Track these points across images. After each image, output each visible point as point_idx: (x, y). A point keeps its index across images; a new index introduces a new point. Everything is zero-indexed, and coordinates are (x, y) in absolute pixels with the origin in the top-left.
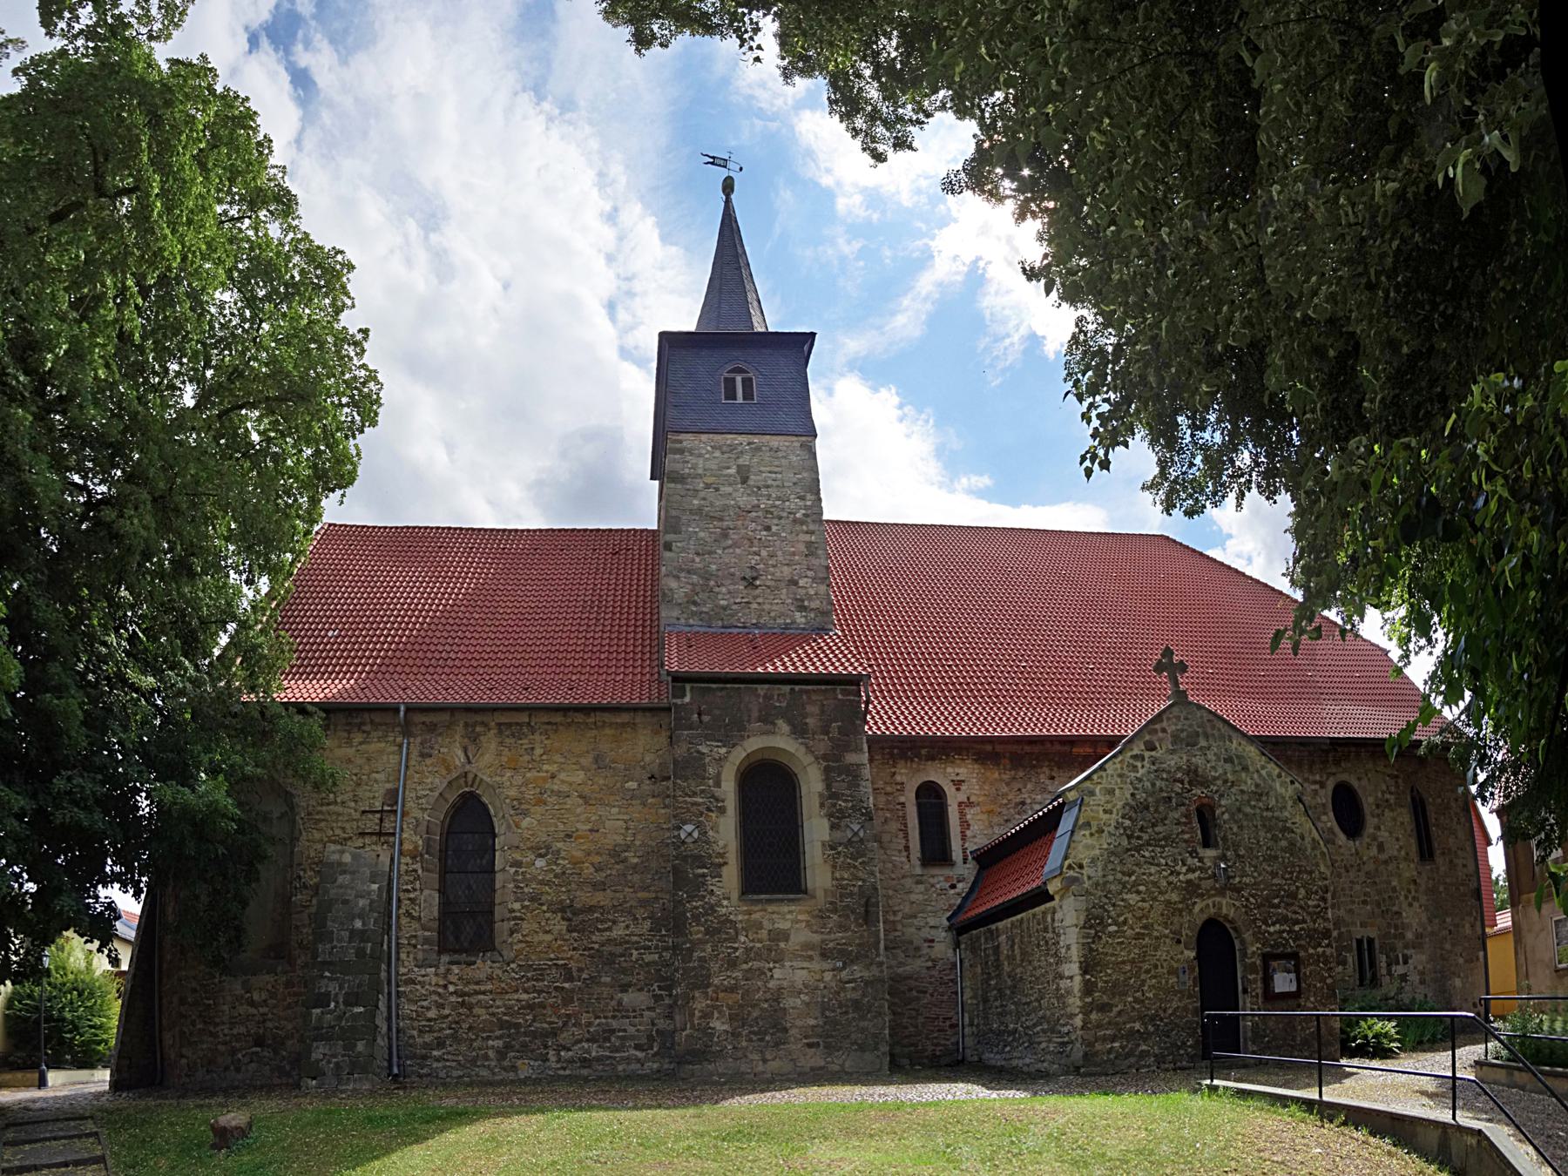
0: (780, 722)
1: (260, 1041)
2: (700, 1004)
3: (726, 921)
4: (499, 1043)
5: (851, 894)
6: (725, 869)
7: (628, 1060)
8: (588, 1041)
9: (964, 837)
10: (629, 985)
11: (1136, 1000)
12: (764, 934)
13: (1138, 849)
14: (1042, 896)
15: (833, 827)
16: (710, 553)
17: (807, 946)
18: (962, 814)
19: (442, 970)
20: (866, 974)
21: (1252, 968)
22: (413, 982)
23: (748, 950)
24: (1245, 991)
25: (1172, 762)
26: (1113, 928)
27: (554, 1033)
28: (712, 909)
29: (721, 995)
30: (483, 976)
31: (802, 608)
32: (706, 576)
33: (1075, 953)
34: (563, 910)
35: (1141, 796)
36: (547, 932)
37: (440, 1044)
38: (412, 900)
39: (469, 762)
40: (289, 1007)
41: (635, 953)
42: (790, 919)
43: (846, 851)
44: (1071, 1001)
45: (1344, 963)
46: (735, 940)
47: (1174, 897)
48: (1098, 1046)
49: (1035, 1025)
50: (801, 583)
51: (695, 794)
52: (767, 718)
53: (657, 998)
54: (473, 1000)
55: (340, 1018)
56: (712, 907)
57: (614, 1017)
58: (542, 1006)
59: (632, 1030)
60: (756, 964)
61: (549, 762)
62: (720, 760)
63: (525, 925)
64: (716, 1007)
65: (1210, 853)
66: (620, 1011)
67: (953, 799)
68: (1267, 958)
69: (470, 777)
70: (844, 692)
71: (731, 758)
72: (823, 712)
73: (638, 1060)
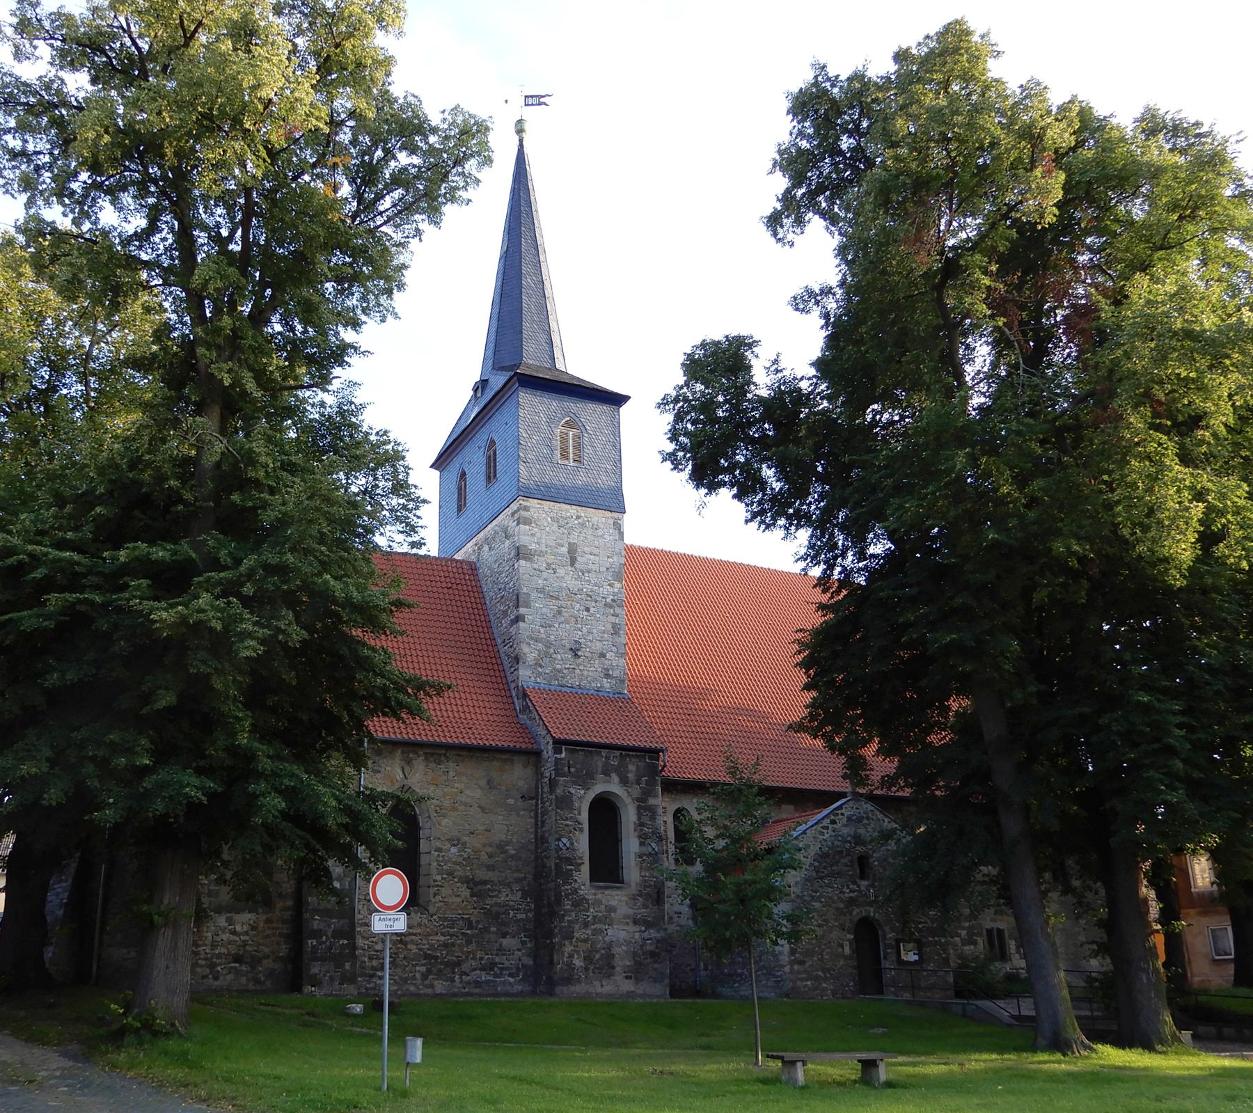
0: (614, 775)
1: (238, 959)
2: (568, 948)
3: (584, 900)
5: (650, 886)
13: (822, 878)
15: (642, 844)
16: (550, 626)
17: (626, 917)
20: (657, 935)
21: (890, 946)
23: (594, 917)
25: (845, 831)
27: (459, 964)
28: (575, 891)
31: (607, 676)
32: (548, 644)
34: (468, 882)
42: (617, 899)
43: (650, 859)
45: (975, 943)
47: (841, 905)
50: (608, 656)
53: (523, 943)
54: (408, 939)
58: (453, 945)
59: (507, 964)
62: (581, 798)
63: (443, 890)
65: (864, 883)
66: (501, 949)
68: (898, 941)
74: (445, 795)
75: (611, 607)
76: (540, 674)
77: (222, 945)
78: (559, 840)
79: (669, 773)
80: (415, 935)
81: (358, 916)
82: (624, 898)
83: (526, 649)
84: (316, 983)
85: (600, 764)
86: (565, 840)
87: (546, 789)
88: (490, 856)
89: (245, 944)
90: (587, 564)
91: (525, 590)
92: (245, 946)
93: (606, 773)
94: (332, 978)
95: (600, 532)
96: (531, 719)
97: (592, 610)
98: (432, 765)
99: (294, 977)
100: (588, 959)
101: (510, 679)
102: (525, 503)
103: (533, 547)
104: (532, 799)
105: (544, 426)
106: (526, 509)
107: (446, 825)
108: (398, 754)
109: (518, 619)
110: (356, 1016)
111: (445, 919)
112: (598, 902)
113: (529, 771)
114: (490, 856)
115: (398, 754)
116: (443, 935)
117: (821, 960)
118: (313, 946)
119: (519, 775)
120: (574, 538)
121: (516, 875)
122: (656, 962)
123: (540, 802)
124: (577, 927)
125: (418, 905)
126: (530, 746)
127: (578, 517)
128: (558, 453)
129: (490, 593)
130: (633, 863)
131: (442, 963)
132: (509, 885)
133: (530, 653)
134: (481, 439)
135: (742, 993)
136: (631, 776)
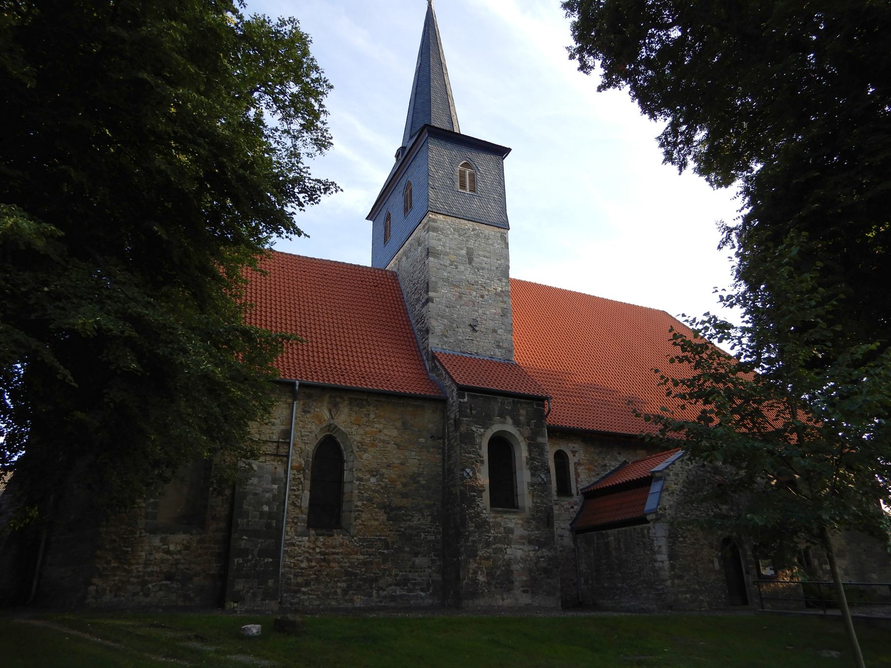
0: (508, 418)
1: (170, 577)
2: (473, 565)
3: (485, 522)
4: (344, 585)
8: (395, 585)
9: (577, 482)
14: (643, 520)
15: (533, 475)
16: (453, 307)
17: (522, 537)
18: (576, 469)
19: (313, 538)
20: (549, 553)
22: (293, 545)
23: (495, 538)
24: (748, 573)
26: (681, 539)
27: (376, 580)
28: (478, 514)
30: (337, 543)
31: (499, 347)
32: (452, 321)
33: (664, 549)
35: (691, 478)
36: (377, 520)
37: (307, 584)
38: (297, 496)
39: (333, 418)
41: (423, 535)
42: (513, 522)
43: (540, 488)
46: (489, 532)
48: (680, 596)
50: (499, 331)
51: (470, 453)
52: (502, 415)
53: (433, 561)
54: (331, 557)
57: (410, 572)
58: (371, 563)
59: (419, 580)
60: (499, 546)
61: (380, 423)
62: (481, 435)
64: (479, 568)
67: (572, 460)
69: (332, 427)
70: (538, 405)
71: (486, 434)
73: (422, 597)
74: (366, 433)
75: (500, 296)
76: (445, 343)
78: (463, 470)
79: (550, 420)
80: (337, 554)
81: (284, 537)
82: (520, 522)
83: (434, 323)
84: (238, 598)
85: (496, 408)
86: (468, 470)
87: (452, 429)
88: (404, 485)
89: (177, 562)
90: (481, 263)
93: (502, 415)
94: (254, 595)
95: (490, 242)
96: (438, 375)
97: (486, 297)
99: (219, 596)
100: (490, 574)
101: (422, 348)
102: (434, 217)
103: (440, 248)
104: (439, 438)
106: (434, 221)
108: (327, 398)
109: (429, 300)
110: (252, 638)
112: (498, 525)
114: (404, 485)
115: (327, 398)
116: (362, 554)
118: (239, 564)
119: (428, 419)
120: (471, 244)
121: (427, 502)
125: (341, 528)
126: (438, 394)
127: (474, 230)
128: (458, 184)
129: (406, 287)
130: (526, 491)
133: (437, 326)
134: (401, 188)
136: (522, 418)
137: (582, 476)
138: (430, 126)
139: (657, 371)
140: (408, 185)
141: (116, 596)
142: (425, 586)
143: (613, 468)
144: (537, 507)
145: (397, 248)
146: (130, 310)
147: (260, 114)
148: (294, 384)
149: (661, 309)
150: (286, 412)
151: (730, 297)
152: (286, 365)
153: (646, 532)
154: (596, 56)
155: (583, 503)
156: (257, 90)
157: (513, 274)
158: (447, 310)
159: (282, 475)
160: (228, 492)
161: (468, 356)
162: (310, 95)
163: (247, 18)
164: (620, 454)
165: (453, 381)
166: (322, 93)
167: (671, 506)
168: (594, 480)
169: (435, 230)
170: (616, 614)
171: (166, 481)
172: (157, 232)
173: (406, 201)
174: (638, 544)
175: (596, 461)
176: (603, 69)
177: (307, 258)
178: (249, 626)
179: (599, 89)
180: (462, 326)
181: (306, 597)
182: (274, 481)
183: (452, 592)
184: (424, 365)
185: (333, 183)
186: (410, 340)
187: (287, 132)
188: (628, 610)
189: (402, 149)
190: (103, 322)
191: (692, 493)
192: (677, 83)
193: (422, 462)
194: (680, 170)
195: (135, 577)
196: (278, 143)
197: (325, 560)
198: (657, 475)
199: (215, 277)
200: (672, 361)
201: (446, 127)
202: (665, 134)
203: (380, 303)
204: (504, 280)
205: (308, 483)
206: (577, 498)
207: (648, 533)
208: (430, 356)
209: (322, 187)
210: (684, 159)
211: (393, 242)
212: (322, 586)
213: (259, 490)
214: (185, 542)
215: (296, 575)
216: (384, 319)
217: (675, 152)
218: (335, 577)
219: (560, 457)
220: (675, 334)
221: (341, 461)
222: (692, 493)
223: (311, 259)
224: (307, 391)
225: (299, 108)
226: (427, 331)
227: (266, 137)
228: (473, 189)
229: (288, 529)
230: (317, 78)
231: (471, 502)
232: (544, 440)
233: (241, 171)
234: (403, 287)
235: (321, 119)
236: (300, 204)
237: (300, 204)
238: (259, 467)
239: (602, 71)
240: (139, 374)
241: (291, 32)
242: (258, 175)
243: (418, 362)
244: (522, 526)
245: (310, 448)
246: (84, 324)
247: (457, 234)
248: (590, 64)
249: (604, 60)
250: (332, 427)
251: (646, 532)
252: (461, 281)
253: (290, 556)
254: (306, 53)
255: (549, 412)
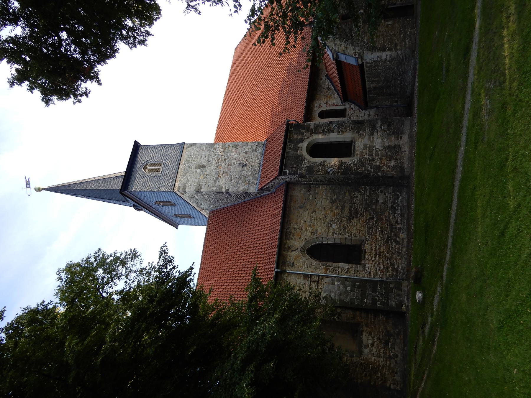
1: (387, 343)
2: (385, 168)
3: (360, 160)
4: (394, 244)
5: (354, 127)
6: (343, 161)
7: (402, 202)
8: (395, 214)
10: (376, 200)
11: (395, 36)
12: (364, 151)
13: (352, 37)
14: (361, 66)
15: (333, 132)
16: (231, 177)
17: (369, 139)
18: (330, 106)
19: (367, 262)
20: (379, 123)
23: (369, 155)
24: (395, 4)
27: (391, 225)
28: (355, 165)
29: (383, 163)
31: (256, 150)
32: (240, 178)
33: (379, 54)
36: (357, 225)
37: (393, 265)
40: (375, 326)
42: (360, 144)
43: (341, 128)
44: (393, 55)
46: (365, 159)
49: (399, 71)
50: (247, 150)
51: (319, 169)
53: (382, 192)
54: (378, 251)
55: (382, 295)
56: (355, 164)
57: (387, 205)
58: (381, 228)
59: (392, 200)
60: (374, 153)
61: (300, 222)
62: (309, 162)
63: (354, 232)
64: (386, 165)
66: (385, 203)
67: (324, 108)
69: (302, 250)
70: (291, 127)
72: (296, 134)
73: (402, 199)
75: (225, 149)
76: (253, 182)
77: (379, 351)
78: (329, 173)
79: (300, 120)
80: (376, 247)
81: (365, 278)
82: (360, 140)
83: (241, 189)
84: (400, 304)
85: (293, 152)
86: (329, 170)
88: (337, 208)
89: (379, 339)
91: (214, 189)
92: (380, 339)
93: (297, 149)
94: (399, 295)
95: (192, 154)
96: (272, 187)
97: (226, 158)
98: (291, 236)
99: (397, 315)
100: (390, 158)
101: (256, 196)
102: (177, 188)
103: (196, 185)
104: (310, 187)
105: (144, 180)
106: (179, 188)
107: (321, 229)
108: (285, 253)
110: (424, 296)
111: (368, 231)
113: (297, 188)
115: (285, 253)
116: (376, 233)
117: (395, 35)
118: (381, 304)
119: (298, 193)
120: (193, 166)
121: (347, 194)
122: (393, 124)
123: (312, 181)
124: (374, 164)
125: (361, 245)
126: (284, 188)
127: (185, 164)
128: (157, 173)
129: (219, 205)
130: (342, 136)
131: (391, 234)
132: (352, 199)
133: (243, 187)
134: (159, 208)
135: (411, 80)
136: (299, 137)
137: (334, 102)
138: (122, 190)
139: (281, 54)
140: (156, 203)
141: (397, 373)
142: (396, 197)
143: (330, 84)
144: (352, 129)
145: (195, 211)
146: (239, 367)
147: (117, 293)
148: (277, 272)
149: (234, 51)
150: (293, 277)
151: (235, 6)
152: (267, 277)
153: (368, 65)
154: (79, 86)
155: (350, 102)
156: (102, 294)
157: (212, 141)
158: (233, 181)
159: (330, 279)
160: (339, 310)
161: (261, 169)
162: (104, 262)
163: (57, 300)
164: (321, 79)
165: (276, 178)
166: (103, 255)
167: (354, 49)
168: (336, 95)
169: (184, 187)
170: (417, 85)
171: (333, 345)
172: (192, 352)
173: (167, 205)
174: (376, 70)
175: (325, 93)
176: (87, 82)
177: (201, 264)
178: (417, 298)
179: (100, 84)
180: (243, 172)
181: (400, 266)
182: (333, 284)
183: (400, 181)
184: (266, 195)
185: (161, 248)
186: (251, 203)
187: (127, 276)
188: (414, 77)
189: (134, 206)
190: (247, 383)
191: (347, 36)
192: (96, 36)
193: (324, 197)
194: (150, 35)
195: (386, 363)
196: (134, 281)
197: (379, 254)
198: (335, 57)
199: (218, 316)
200: (273, 44)
201: (121, 180)
202: (128, 44)
203: (229, 221)
204: (215, 146)
205: (335, 264)
206: (347, 106)
207: (369, 63)
208: (262, 191)
209: (164, 255)
210: (144, 32)
211: (191, 213)
212: (394, 257)
213: (338, 292)
214: (367, 335)
215: (388, 271)
216: (238, 218)
217: (139, 38)
218: (389, 249)
219: (323, 115)
220: (258, 42)
221: (322, 244)
222: (347, 36)
223: (201, 262)
224: (281, 264)
225: (112, 269)
226: (246, 193)
227: (130, 289)
228: (160, 164)
229: (361, 275)
230: (94, 258)
231: (348, 169)
232: (312, 124)
233: (155, 303)
234: (219, 207)
235: (119, 255)
236: (174, 268)
237: (174, 268)
238: (325, 292)
239: (89, 82)
240: (277, 361)
241: (66, 274)
242: (156, 293)
243: (264, 199)
244: (363, 139)
245: (315, 263)
246: (248, 394)
247: (187, 174)
248: (84, 89)
249: (82, 80)
250: (302, 250)
251: (368, 65)
252: (216, 172)
253: (377, 275)
254: (79, 265)
255: (295, 121)
